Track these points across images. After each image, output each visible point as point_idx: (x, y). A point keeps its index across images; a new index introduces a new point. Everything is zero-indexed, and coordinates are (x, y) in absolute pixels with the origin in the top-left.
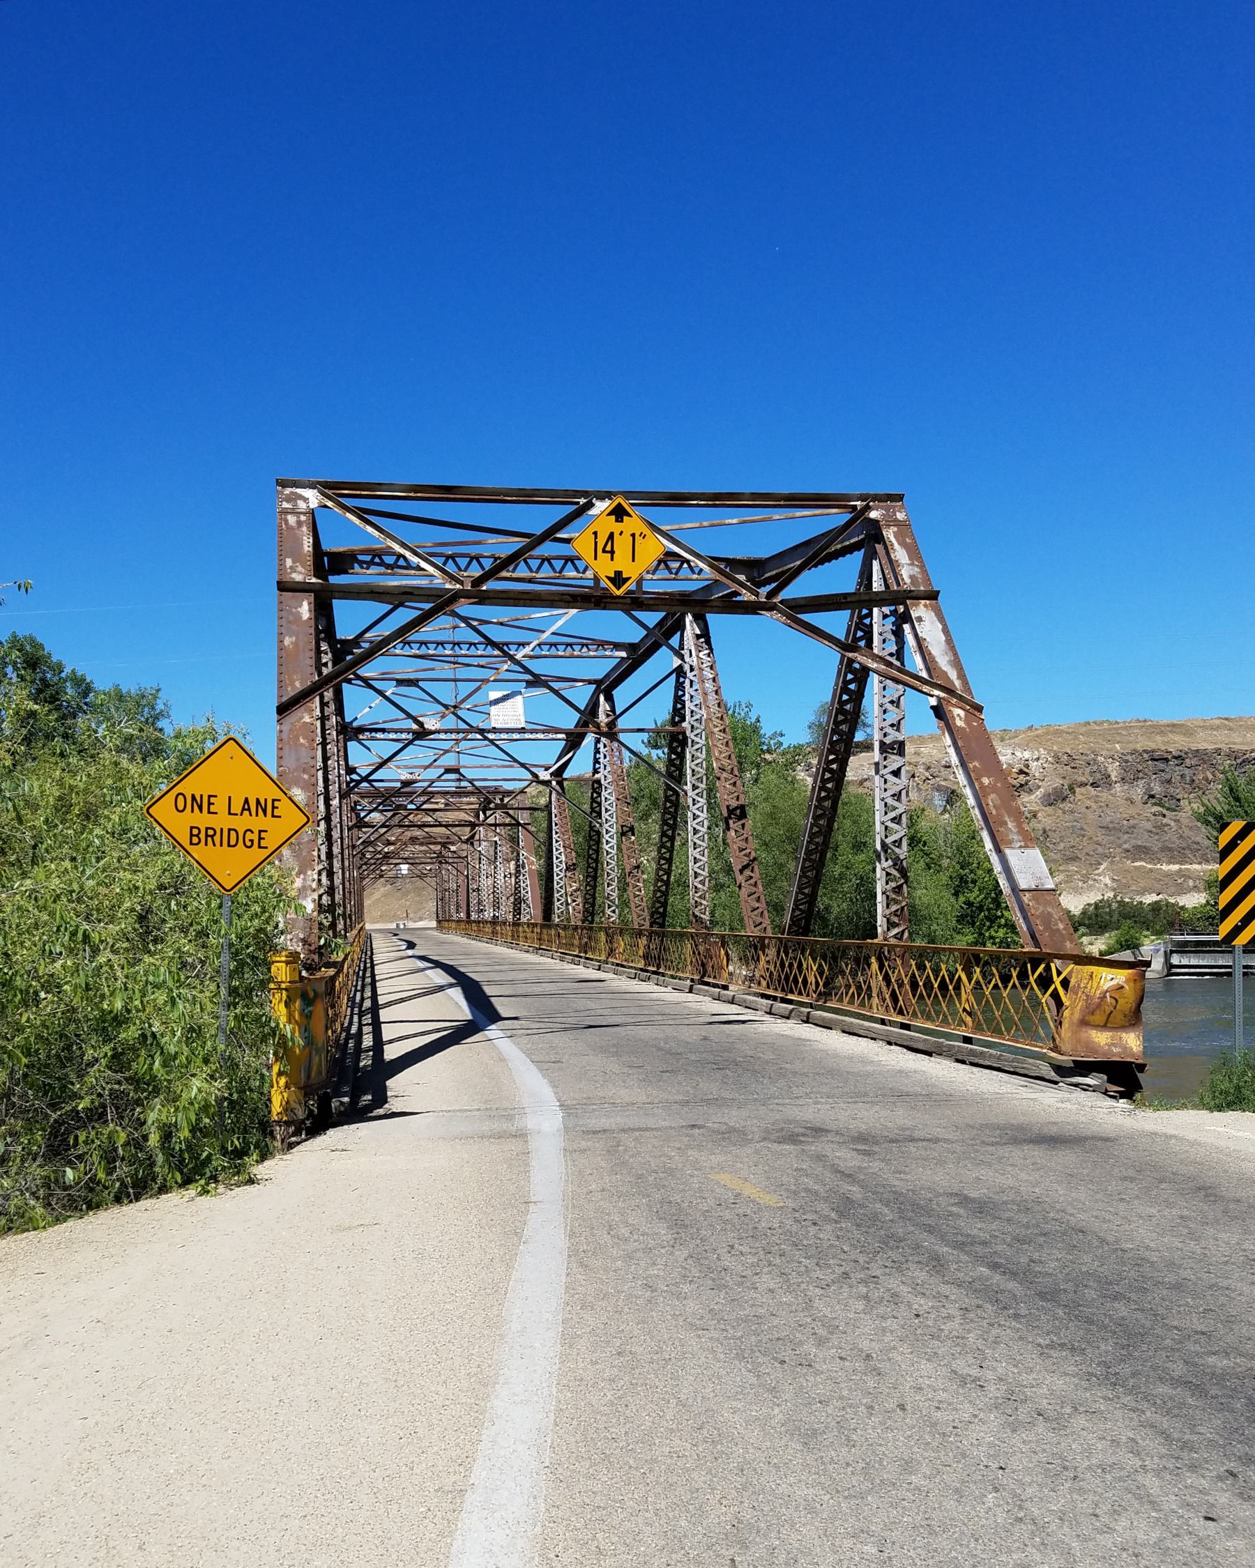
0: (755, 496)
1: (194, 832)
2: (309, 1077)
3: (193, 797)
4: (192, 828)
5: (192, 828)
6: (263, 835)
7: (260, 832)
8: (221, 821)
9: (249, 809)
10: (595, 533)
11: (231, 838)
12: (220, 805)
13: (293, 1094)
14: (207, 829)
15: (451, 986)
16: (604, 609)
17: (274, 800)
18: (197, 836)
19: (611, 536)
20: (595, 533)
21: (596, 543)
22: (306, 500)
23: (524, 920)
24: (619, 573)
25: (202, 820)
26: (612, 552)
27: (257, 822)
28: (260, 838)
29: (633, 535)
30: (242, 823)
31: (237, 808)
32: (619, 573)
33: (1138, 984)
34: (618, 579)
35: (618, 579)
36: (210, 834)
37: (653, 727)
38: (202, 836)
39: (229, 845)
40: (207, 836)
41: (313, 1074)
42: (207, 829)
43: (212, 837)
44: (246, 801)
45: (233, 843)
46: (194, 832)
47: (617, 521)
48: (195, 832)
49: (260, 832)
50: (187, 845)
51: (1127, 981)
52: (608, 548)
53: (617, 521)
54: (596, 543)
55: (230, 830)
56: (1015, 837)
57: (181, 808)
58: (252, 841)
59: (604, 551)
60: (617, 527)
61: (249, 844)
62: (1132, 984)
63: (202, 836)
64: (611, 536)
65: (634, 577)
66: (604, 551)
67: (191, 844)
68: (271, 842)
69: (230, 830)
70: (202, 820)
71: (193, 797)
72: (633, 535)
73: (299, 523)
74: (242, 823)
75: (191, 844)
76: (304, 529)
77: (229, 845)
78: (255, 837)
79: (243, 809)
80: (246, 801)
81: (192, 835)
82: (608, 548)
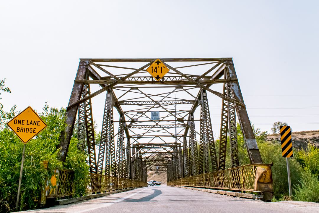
1: (18, 129)
2: (49, 193)
3: (19, 120)
4: (18, 128)
5: (18, 128)
6: (35, 130)
7: (34, 129)
8: (25, 126)
9: (32, 124)
10: (152, 67)
11: (27, 130)
12: (25, 122)
14: (21, 128)
17: (38, 121)
18: (19, 130)
19: (156, 68)
20: (152, 67)
21: (152, 69)
22: (86, 63)
24: (158, 76)
25: (20, 126)
26: (156, 71)
27: (33, 126)
28: (34, 130)
29: (161, 67)
30: (30, 127)
31: (29, 123)
32: (158, 76)
33: (270, 171)
36: (22, 129)
38: (20, 130)
39: (26, 132)
40: (21, 130)
41: (50, 193)
42: (21, 128)
43: (22, 130)
44: (31, 121)
45: (27, 131)
46: (18, 129)
47: (157, 64)
48: (18, 129)
49: (34, 129)
50: (16, 132)
51: (267, 170)
52: (155, 70)
53: (157, 64)
54: (152, 69)
55: (27, 128)
56: (250, 136)
57: (15, 123)
58: (32, 131)
59: (154, 71)
60: (157, 66)
61: (31, 132)
62: (268, 171)
63: (20, 130)
64: (156, 68)
66: (154, 71)
67: (17, 131)
68: (36, 131)
69: (27, 128)
70: (20, 126)
71: (19, 120)
72: (161, 67)
73: (83, 68)
74: (30, 127)
75: (17, 131)
76: (84, 69)
77: (26, 132)
78: (33, 130)
79: (31, 123)
80: (31, 121)
81: (17, 130)
82: (155, 70)
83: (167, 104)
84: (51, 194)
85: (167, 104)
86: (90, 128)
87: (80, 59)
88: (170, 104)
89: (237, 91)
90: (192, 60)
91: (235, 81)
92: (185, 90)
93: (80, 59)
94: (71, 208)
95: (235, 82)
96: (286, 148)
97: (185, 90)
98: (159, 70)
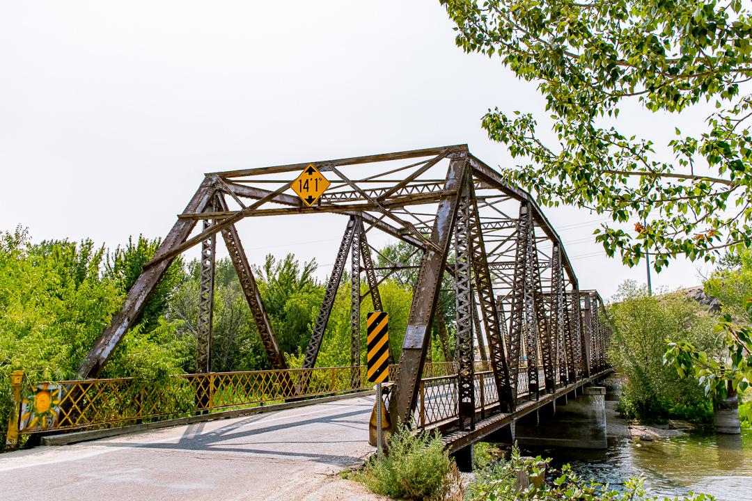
0: (310, 423)
10: (300, 181)
13: (712, 386)
15: (547, 238)
16: (304, 213)
19: (307, 181)
23: (349, 365)
24: (310, 197)
26: (308, 188)
29: (316, 180)
32: (310, 197)
34: (310, 200)
35: (310, 200)
37: (623, 97)
41: (31, 425)
52: (306, 186)
59: (304, 188)
64: (307, 181)
65: (317, 198)
66: (304, 188)
72: (316, 180)
82: (306, 186)
83: (494, 228)
84: (33, 427)
85: (494, 228)
86: (478, 253)
87: (514, 157)
88: (498, 229)
89: (444, 217)
90: (390, 157)
91: (449, 195)
92: (490, 205)
93: (514, 157)
94: (7, 459)
95: (448, 199)
96: (375, 362)
97: (490, 205)
98: (312, 184)
